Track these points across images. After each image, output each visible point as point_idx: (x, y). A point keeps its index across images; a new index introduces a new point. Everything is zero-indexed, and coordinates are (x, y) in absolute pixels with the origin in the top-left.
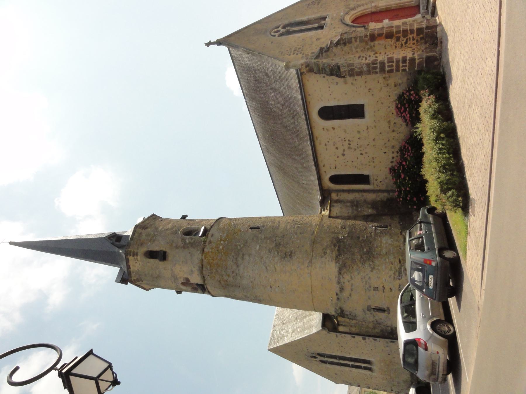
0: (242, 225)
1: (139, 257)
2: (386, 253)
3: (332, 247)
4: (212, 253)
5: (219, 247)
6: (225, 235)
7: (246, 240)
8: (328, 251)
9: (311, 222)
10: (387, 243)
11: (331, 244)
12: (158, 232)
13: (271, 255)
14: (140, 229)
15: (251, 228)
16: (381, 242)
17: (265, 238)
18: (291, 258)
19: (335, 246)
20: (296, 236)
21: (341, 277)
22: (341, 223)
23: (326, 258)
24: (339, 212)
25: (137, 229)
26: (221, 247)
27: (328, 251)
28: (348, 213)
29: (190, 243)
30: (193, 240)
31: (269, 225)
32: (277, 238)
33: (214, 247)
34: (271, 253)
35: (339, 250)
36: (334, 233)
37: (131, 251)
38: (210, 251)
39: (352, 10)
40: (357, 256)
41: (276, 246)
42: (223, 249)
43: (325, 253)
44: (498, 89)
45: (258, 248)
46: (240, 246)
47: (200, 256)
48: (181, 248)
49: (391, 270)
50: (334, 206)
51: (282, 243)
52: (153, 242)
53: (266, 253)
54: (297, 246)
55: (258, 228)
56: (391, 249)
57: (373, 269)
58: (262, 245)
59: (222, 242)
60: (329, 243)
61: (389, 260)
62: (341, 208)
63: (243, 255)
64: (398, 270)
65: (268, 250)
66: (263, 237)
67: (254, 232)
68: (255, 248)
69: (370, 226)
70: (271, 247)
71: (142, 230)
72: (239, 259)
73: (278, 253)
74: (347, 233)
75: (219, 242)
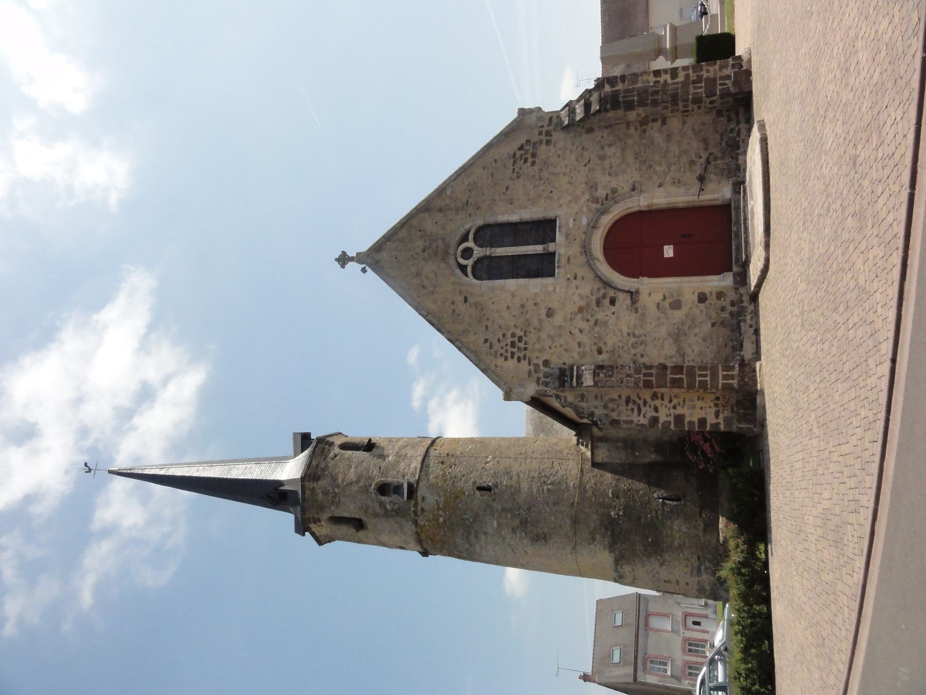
0: (463, 479)
1: (323, 523)
2: (680, 546)
3: (603, 530)
4: (430, 526)
5: (439, 520)
6: (442, 499)
7: (476, 512)
8: (598, 537)
9: (567, 478)
10: (680, 531)
11: (600, 525)
12: (338, 486)
13: (516, 536)
14: (310, 481)
15: (480, 489)
16: (672, 529)
17: (504, 510)
18: (546, 541)
19: (607, 529)
20: (547, 509)
21: (619, 567)
22: (611, 484)
23: (595, 546)
24: (606, 457)
25: (306, 483)
26: (441, 520)
27: (598, 537)
28: (621, 459)
29: (393, 510)
30: (396, 505)
31: (504, 483)
32: (521, 511)
33: (431, 519)
34: (516, 533)
35: (613, 536)
36: (602, 505)
37: (309, 518)
38: (426, 524)
39: (603, 214)
40: (639, 548)
41: (521, 523)
42: (445, 521)
43: (593, 539)
44: (865, 600)
45: (495, 524)
46: (469, 521)
47: (413, 528)
48: (383, 516)
49: (687, 566)
50: (598, 447)
51: (529, 520)
52: (337, 505)
53: (508, 532)
54: (553, 527)
55: (488, 489)
56: (687, 542)
57: (661, 565)
58: (500, 521)
59: (441, 513)
60: (598, 523)
61: (683, 555)
62: (609, 450)
63: (476, 532)
64: (696, 568)
65: (511, 529)
66: (500, 509)
67: (485, 498)
68: (493, 525)
69: (655, 495)
70: (515, 525)
71: (313, 483)
72: (472, 538)
73: (526, 533)
74: (622, 508)
75: (436, 512)
